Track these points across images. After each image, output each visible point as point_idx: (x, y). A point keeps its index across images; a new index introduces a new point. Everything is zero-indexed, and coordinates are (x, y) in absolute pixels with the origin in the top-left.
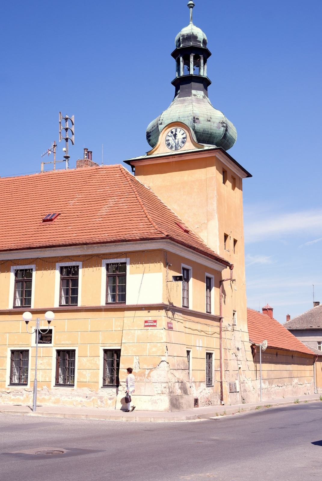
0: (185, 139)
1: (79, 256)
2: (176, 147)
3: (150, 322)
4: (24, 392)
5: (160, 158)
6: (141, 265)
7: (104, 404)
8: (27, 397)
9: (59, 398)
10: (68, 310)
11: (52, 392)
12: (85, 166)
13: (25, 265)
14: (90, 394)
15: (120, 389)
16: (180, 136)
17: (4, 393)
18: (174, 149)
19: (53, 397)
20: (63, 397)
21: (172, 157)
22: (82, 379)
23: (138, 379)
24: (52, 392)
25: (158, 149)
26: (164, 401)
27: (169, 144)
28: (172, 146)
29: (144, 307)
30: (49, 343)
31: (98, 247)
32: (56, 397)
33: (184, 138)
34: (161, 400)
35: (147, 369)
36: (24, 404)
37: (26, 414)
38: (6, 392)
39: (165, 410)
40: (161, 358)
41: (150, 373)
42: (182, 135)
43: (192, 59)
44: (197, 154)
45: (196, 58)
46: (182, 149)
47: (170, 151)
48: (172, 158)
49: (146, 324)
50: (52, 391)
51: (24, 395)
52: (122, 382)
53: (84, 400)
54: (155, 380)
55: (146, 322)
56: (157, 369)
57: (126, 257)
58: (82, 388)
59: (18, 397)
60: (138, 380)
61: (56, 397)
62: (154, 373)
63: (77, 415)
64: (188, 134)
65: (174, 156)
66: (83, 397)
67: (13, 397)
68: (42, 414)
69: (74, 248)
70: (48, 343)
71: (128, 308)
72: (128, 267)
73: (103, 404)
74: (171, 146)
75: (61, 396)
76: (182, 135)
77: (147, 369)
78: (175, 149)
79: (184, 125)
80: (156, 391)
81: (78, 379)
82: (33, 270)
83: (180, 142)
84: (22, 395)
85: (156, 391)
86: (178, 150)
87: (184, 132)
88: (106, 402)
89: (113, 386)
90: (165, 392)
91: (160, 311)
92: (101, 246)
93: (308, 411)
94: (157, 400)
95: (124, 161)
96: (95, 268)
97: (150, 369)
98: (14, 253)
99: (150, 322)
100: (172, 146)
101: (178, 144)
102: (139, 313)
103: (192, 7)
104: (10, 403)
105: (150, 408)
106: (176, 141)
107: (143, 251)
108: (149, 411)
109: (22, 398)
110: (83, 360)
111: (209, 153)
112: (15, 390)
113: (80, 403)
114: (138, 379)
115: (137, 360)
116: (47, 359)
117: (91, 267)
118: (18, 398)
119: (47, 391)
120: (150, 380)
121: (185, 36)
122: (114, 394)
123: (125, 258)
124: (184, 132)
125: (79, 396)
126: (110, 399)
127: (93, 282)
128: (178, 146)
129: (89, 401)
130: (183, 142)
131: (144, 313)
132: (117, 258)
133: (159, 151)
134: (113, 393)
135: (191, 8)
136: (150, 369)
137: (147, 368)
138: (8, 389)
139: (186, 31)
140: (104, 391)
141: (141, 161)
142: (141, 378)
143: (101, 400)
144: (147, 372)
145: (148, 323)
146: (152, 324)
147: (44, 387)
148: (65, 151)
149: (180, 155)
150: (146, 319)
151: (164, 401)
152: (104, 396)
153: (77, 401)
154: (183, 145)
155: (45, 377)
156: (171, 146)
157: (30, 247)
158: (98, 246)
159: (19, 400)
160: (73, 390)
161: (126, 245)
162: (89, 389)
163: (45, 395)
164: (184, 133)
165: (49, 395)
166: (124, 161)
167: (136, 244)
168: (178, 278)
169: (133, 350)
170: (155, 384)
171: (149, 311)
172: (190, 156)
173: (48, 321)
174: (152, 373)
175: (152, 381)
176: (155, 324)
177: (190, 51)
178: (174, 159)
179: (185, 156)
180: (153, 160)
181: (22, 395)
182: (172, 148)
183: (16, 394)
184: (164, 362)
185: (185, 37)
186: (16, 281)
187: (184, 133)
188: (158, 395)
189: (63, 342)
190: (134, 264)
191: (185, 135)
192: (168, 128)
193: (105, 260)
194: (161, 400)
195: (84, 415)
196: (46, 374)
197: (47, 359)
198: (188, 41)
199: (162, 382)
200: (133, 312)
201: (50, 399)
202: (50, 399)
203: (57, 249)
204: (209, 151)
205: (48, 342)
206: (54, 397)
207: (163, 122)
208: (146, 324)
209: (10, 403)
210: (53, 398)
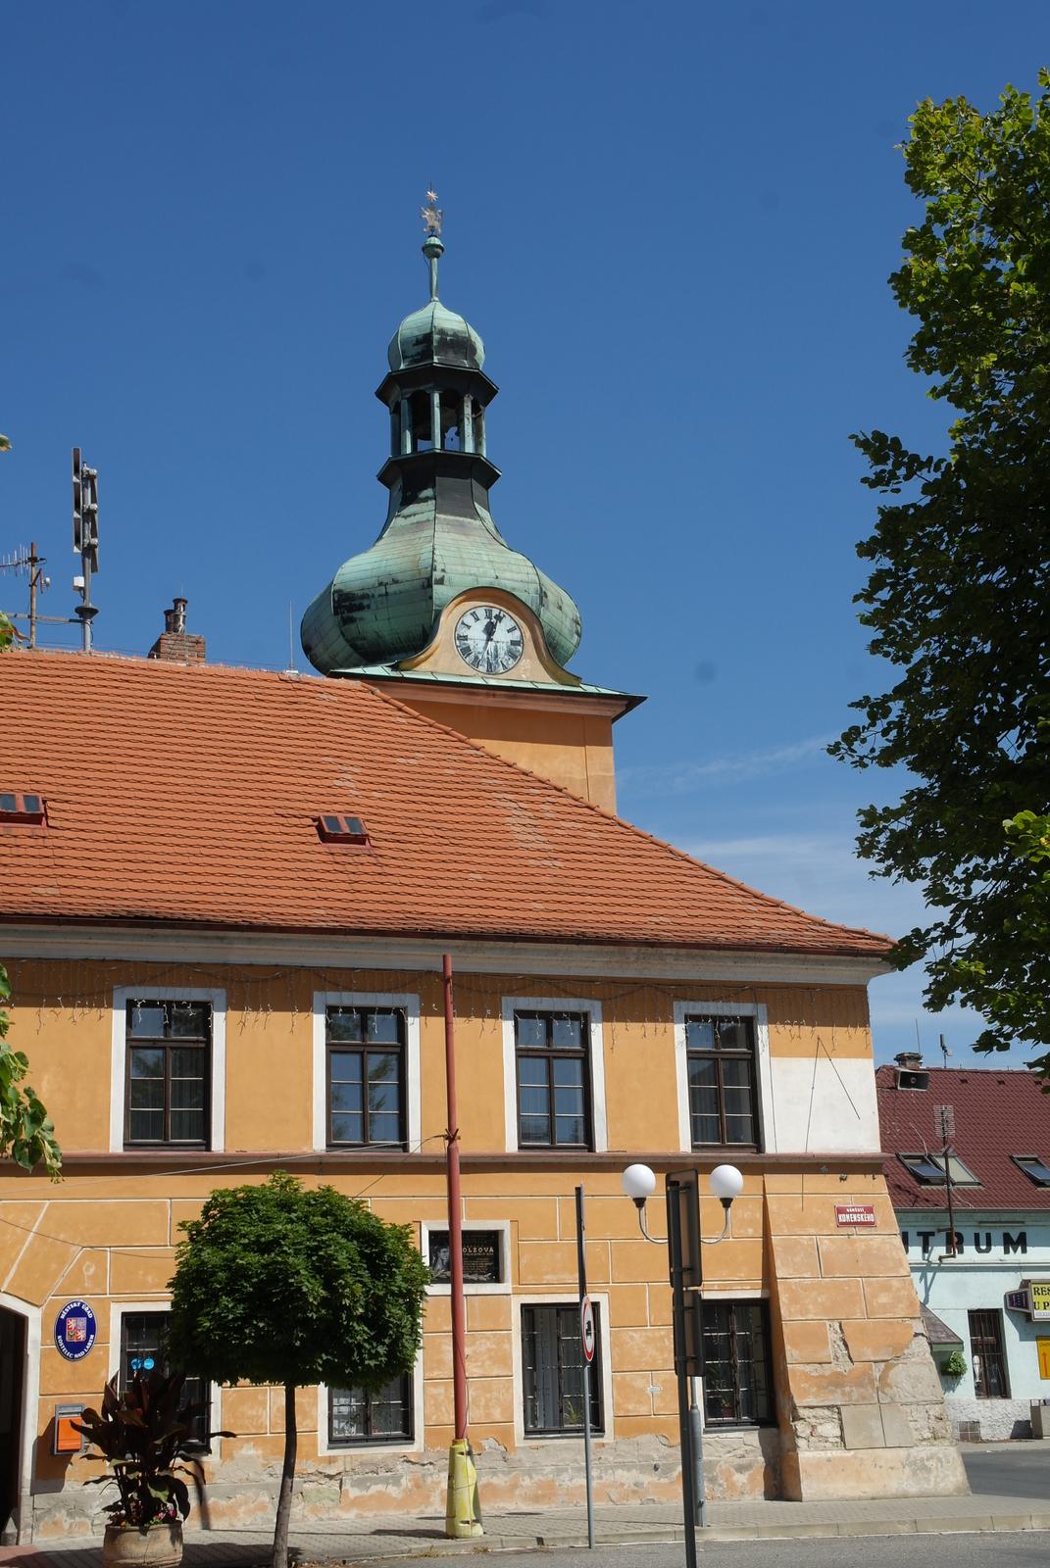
0: (520, 648)
1: (591, 980)
2: (490, 665)
3: (853, 1213)
4: (401, 1468)
5: (614, 702)
6: (806, 1029)
7: (721, 1489)
8: (418, 1486)
9: (553, 1481)
10: (560, 1164)
11: (520, 1461)
12: (196, 658)
13: (379, 992)
14: (664, 1457)
15: (803, 1432)
16: (503, 635)
17: (313, 1478)
18: (483, 668)
19: (526, 1478)
20: (565, 1477)
21: (485, 691)
22: (630, 1407)
23: (855, 1396)
24: (520, 1461)
25: (431, 659)
26: (948, 1462)
27: (466, 651)
28: (476, 658)
29: (824, 1164)
30: (484, 1282)
31: (677, 957)
32: (537, 1478)
33: (513, 643)
34: (939, 1460)
35: (875, 1362)
36: (408, 1513)
37: (659, 1539)
38: (321, 1473)
39: (958, 1490)
40: (910, 1326)
41: (888, 1376)
42: (509, 631)
43: (468, 410)
44: (565, 702)
45: (452, 405)
46: (511, 674)
47: (470, 671)
48: (488, 695)
49: (843, 1218)
50: (520, 1455)
51: (403, 1481)
52: (805, 1407)
53: (647, 1479)
54: (906, 1396)
55: (841, 1211)
56: (905, 1361)
57: (756, 1001)
58: (635, 1439)
59: (374, 1489)
60: (853, 1398)
61: (537, 1478)
62: (898, 1374)
63: (882, 1523)
64: (528, 635)
65: (492, 692)
66: (642, 1469)
67: (354, 1492)
68: (757, 1530)
69: (590, 952)
70: (479, 1281)
71: (774, 1164)
72: (763, 1032)
73: (716, 1487)
74: (472, 656)
75: (559, 1471)
76: (509, 631)
77: (875, 1362)
78: (488, 670)
79: (516, 601)
80: (916, 1430)
81: (616, 1406)
82: (409, 1010)
83: (502, 653)
84: (397, 1481)
85: (916, 1430)
86: (496, 674)
87: (513, 624)
88: (727, 1480)
89: (736, 1424)
90: (944, 1431)
91: (876, 1176)
92: (688, 956)
93: (479, 1491)
94: (928, 1460)
95: (645, 698)
96: (650, 1026)
97: (883, 1361)
98: (347, 942)
99: (856, 1213)
100: (476, 658)
101: (496, 656)
102: (813, 1181)
103: (438, 256)
104: (344, 1515)
105: (913, 1488)
106: (491, 645)
107: (809, 988)
108: (913, 1497)
109: (393, 1491)
110: (632, 1338)
111: (599, 704)
112: (361, 1464)
113: (634, 1492)
114: (855, 1396)
115: (836, 1333)
116: (488, 1338)
117: (641, 1020)
118: (379, 1492)
119: (501, 1458)
120: (892, 1398)
121: (447, 335)
122: (752, 1451)
123: (752, 1002)
124: (513, 624)
125: (624, 1466)
126: (740, 1469)
127: (641, 1075)
128: (497, 663)
129: (666, 1481)
130: (513, 655)
131: (827, 1182)
132: (727, 999)
133: (436, 662)
134: (748, 1448)
135: (436, 259)
136: (883, 1361)
137: (877, 1358)
138: (331, 1460)
139: (413, 323)
140: (714, 1444)
141: (385, 683)
142: (862, 1390)
143: (711, 1475)
144: (877, 1371)
145: (848, 1216)
146: (861, 1218)
147: (485, 1443)
148: (81, 589)
149: (512, 693)
150: (839, 1201)
151: (948, 1462)
152: (719, 1462)
153: (622, 1485)
154: (511, 662)
155: (487, 1407)
156: (472, 656)
157: (430, 929)
158: (678, 954)
159: (382, 1500)
160: (603, 1445)
161: (771, 963)
162: (660, 1437)
163: (494, 1474)
164: (513, 629)
165: (509, 1473)
166: (645, 698)
167: (804, 962)
168: (913, 1080)
169: (819, 1300)
170: (907, 1409)
171: (844, 1176)
172: (543, 703)
173: (722, 1200)
174: (892, 1373)
175: (897, 1399)
176: (870, 1218)
177: (430, 385)
178: (491, 699)
179: (527, 698)
180: (424, 689)
181: (397, 1481)
182: (476, 663)
183: (367, 1479)
184: (920, 1337)
185: (448, 338)
186: (691, 1055)
187: (513, 629)
188: (924, 1443)
189: (548, 1278)
190: (783, 1023)
191: (517, 633)
192: (464, 601)
193: (684, 1004)
194: (939, 1460)
195: (904, 1523)
196: (488, 1395)
197: (488, 1338)
198: (456, 353)
199: (927, 1402)
200: (797, 1178)
201: (515, 1486)
202: (515, 1486)
203: (526, 950)
204: (602, 701)
205: (481, 1278)
206: (531, 1478)
207: (446, 579)
208: (843, 1218)
209: (344, 1515)
210: (526, 1482)
